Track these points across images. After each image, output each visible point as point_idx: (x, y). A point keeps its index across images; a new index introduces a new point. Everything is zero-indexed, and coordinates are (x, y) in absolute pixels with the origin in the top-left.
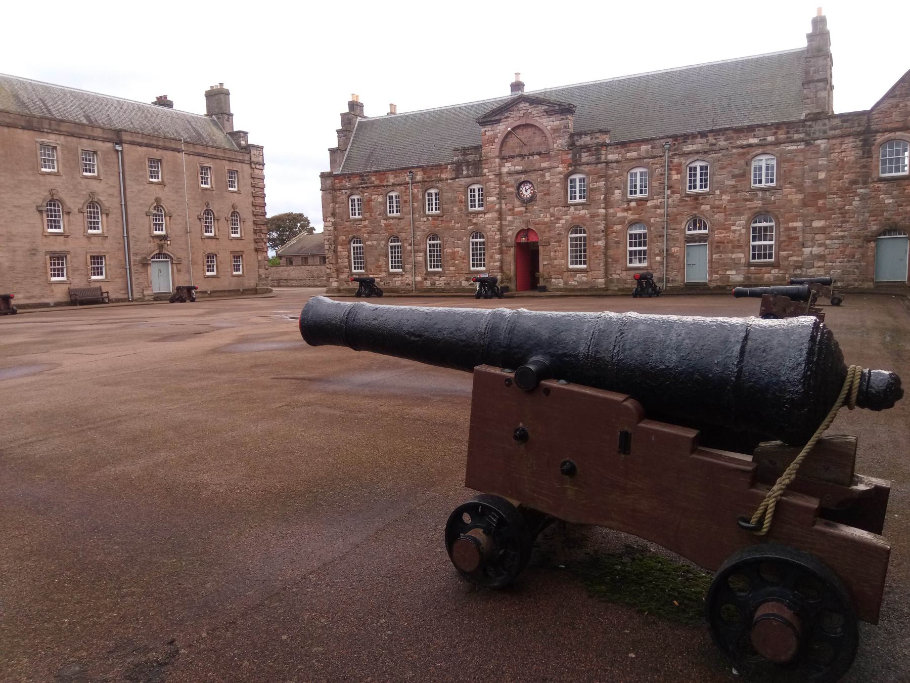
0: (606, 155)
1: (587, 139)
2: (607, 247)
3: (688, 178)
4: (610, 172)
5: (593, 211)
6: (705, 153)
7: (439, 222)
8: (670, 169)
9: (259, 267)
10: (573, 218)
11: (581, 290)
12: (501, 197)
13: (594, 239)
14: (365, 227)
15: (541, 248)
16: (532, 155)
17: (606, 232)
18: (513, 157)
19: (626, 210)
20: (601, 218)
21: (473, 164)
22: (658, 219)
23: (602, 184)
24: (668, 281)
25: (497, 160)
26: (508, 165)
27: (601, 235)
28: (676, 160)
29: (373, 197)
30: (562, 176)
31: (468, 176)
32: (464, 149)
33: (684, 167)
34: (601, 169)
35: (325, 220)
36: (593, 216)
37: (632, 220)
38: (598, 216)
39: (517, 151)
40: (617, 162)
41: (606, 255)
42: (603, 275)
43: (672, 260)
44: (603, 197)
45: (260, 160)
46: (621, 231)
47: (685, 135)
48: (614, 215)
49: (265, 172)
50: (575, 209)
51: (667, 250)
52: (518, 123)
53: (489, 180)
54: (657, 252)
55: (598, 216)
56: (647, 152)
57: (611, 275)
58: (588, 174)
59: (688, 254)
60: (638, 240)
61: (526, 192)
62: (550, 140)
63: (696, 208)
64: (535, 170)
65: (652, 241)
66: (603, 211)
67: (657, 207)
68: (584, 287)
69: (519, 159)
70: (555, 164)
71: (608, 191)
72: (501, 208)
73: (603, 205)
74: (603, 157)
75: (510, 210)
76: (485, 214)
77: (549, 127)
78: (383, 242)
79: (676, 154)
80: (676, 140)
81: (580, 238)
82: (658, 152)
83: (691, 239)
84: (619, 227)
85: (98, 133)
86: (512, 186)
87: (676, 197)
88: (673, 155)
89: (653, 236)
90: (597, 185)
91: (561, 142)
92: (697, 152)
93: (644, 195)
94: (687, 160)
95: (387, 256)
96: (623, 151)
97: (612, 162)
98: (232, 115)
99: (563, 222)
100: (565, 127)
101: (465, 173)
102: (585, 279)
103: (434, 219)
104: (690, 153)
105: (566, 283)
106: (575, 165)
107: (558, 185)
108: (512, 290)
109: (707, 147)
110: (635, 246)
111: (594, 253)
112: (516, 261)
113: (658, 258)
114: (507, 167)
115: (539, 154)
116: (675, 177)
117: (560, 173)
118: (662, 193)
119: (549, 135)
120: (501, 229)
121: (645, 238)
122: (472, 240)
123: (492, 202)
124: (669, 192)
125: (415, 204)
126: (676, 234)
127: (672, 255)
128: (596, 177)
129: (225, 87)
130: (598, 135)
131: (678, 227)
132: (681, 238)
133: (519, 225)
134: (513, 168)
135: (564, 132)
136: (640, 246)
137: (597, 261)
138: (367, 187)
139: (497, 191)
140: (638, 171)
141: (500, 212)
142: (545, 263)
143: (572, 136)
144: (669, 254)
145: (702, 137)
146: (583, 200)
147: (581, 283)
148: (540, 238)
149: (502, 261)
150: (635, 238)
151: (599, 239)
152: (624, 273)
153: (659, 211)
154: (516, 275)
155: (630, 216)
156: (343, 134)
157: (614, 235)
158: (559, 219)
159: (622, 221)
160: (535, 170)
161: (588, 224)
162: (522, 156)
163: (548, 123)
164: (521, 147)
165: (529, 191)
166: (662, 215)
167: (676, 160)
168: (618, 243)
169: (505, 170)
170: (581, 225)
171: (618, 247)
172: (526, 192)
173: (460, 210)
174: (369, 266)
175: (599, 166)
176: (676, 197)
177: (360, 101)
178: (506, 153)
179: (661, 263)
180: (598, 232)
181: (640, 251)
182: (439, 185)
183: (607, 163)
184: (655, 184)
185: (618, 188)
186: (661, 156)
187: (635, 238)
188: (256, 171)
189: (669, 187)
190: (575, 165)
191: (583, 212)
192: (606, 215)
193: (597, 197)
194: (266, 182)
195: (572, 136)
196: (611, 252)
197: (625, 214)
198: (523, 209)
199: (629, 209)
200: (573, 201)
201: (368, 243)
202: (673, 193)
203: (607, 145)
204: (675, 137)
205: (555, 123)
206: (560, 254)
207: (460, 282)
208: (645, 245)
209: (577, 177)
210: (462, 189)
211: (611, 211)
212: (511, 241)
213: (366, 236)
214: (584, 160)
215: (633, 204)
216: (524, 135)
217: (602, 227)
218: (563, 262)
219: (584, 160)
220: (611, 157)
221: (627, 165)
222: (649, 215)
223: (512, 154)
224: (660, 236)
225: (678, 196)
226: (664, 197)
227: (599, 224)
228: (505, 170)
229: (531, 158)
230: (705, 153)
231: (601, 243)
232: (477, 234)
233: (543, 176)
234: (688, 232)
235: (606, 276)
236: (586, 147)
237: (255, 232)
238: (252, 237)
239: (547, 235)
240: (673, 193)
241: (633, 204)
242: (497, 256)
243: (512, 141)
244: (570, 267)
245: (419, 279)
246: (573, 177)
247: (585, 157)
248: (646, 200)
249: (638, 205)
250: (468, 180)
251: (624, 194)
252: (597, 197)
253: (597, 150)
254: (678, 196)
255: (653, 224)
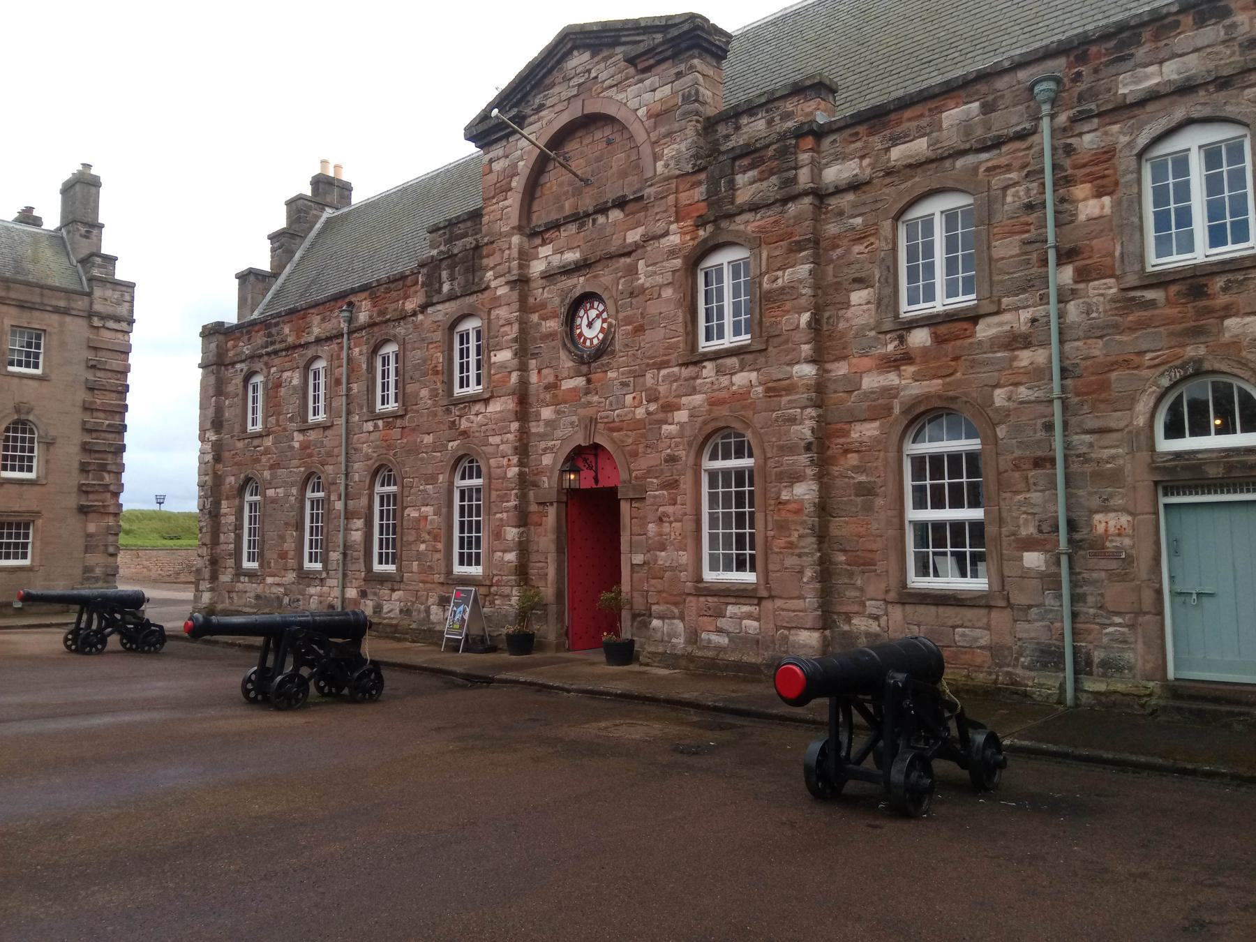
0: (817, 169)
1: (756, 127)
2: (824, 508)
3: (908, 483)
4: (832, 229)
5: (776, 372)
6: (1223, 83)
7: (396, 433)
8: (1063, 181)
9: (87, 549)
10: (713, 403)
11: (738, 666)
12: (523, 352)
13: (780, 477)
14: (267, 451)
15: (625, 507)
16: (603, 210)
17: (822, 448)
18: (556, 226)
19: (893, 363)
20: (802, 397)
21: (463, 261)
22: (1023, 392)
23: (803, 270)
24: (1083, 666)
25: (516, 239)
26: (545, 251)
27: (804, 459)
28: (1089, 141)
29: (286, 375)
30: (678, 263)
31: (452, 297)
32: (451, 224)
33: (1125, 161)
34: (798, 219)
35: (202, 439)
36: (774, 390)
37: (918, 400)
38: (791, 389)
39: (568, 207)
40: (855, 186)
41: (822, 536)
42: (811, 617)
43: (1097, 570)
44: (805, 317)
45: (122, 310)
46: (877, 444)
47: (1122, 27)
48: (852, 384)
49: (134, 338)
50: (719, 371)
51: (1072, 526)
52: (564, 119)
53: (496, 302)
54: (1029, 530)
55: (791, 389)
56: (966, 127)
57: (848, 617)
58: (755, 243)
59: (1175, 551)
60: (952, 479)
61: (591, 329)
62: (646, 150)
63: (1196, 333)
64: (611, 257)
65: (1001, 486)
66: (808, 370)
67: (1016, 341)
68: (750, 658)
69: (572, 228)
70: (660, 227)
71: (826, 301)
72: (524, 383)
73: (806, 349)
74: (804, 176)
75: (548, 387)
76: (486, 401)
77: (642, 112)
78: (294, 491)
79: (1085, 116)
80: (1083, 59)
81: (740, 474)
82: (1011, 119)
83: (1184, 476)
84: (868, 431)
85: (49, 308)
86: (554, 315)
87: (1102, 291)
88: (1074, 120)
89: (1005, 461)
90: (785, 277)
91: (678, 150)
92: (1185, 89)
93: (965, 300)
94: (1135, 130)
95: (299, 526)
96: (876, 142)
97: (839, 191)
98: (101, 226)
99: (682, 416)
100: (686, 99)
101: (446, 288)
102: (751, 625)
103: (388, 426)
104: (1153, 96)
105: (693, 637)
106: (715, 223)
107: (668, 293)
108: (542, 647)
109: (1229, 59)
110: (938, 504)
111: (782, 527)
112: (559, 550)
113: (1033, 560)
114: (545, 258)
115: (621, 203)
116: (1090, 207)
117: (672, 253)
118: (1034, 284)
119: (641, 136)
120: (523, 449)
121: (974, 470)
122: (460, 483)
123: (503, 366)
124: (1067, 274)
125: (355, 386)
126: (1111, 451)
127: (1097, 547)
128: (780, 249)
129: (93, 171)
130: (789, 106)
131: (1115, 419)
132: (1136, 470)
133: (570, 435)
134: (556, 260)
135: (686, 114)
136: (957, 503)
137: (791, 561)
138: (275, 352)
139: (513, 331)
140: (936, 207)
141: (523, 397)
142: (638, 559)
143: (710, 125)
144: (1082, 543)
145: (1201, 22)
146: (745, 339)
147: (740, 640)
148: (624, 476)
149: (523, 548)
150: (937, 473)
151: (795, 478)
152: (896, 613)
153: (1025, 358)
154: (559, 595)
155: (910, 385)
156: (282, 242)
157: (853, 459)
158: (669, 408)
159: (879, 407)
160: (611, 257)
161: (758, 420)
162: (578, 218)
163: (637, 99)
164: (577, 193)
165: (598, 324)
166: (1038, 374)
167: (1089, 141)
168: (867, 491)
169: (537, 267)
170: (737, 426)
171: (868, 508)
172: (591, 329)
173: (433, 394)
174: (268, 554)
175: (792, 208)
176: (1102, 291)
177: (345, 177)
178: (540, 217)
179: (1050, 581)
180: (790, 449)
181: (958, 526)
182: (400, 330)
183: (820, 195)
184: (1007, 248)
185: (861, 282)
186: (1021, 136)
187: (937, 473)
188: (106, 335)
189: (1065, 256)
190: (715, 223)
191: (741, 379)
192: (820, 388)
193: (786, 322)
194: (133, 359)
195: (710, 125)
196: (841, 527)
197: (892, 379)
198: (580, 382)
199: (906, 358)
200: (716, 345)
201: (270, 493)
202: (1083, 275)
203: (819, 133)
204: (1076, 49)
205: (659, 94)
206: (673, 530)
207: (428, 611)
208: (974, 504)
209: (724, 258)
210: (438, 336)
211: (840, 369)
212: (547, 483)
213: (267, 474)
214: (743, 197)
215: (920, 338)
216: (582, 152)
217: (804, 430)
218: (684, 557)
219: (743, 197)
220: (834, 174)
221: (891, 195)
222: (984, 376)
223: (554, 216)
224: (1038, 463)
225: (1110, 287)
226: (1044, 299)
227: (792, 420)
228: (537, 267)
229: (601, 219)
230: (1223, 83)
231: (805, 491)
232: (466, 463)
233: (632, 271)
234: (1167, 446)
235: (826, 620)
236: (751, 154)
237: (84, 469)
238: (75, 479)
239: (643, 464)
240: (1083, 275)
241: (920, 338)
242: (512, 533)
243: (555, 179)
244: (709, 576)
245: (352, 593)
246: (713, 261)
247: (747, 186)
248: (972, 317)
249: (938, 340)
250: (451, 308)
251: (887, 302)
252: (786, 322)
253: (783, 152)
254: (1110, 287)
255: (1006, 414)
